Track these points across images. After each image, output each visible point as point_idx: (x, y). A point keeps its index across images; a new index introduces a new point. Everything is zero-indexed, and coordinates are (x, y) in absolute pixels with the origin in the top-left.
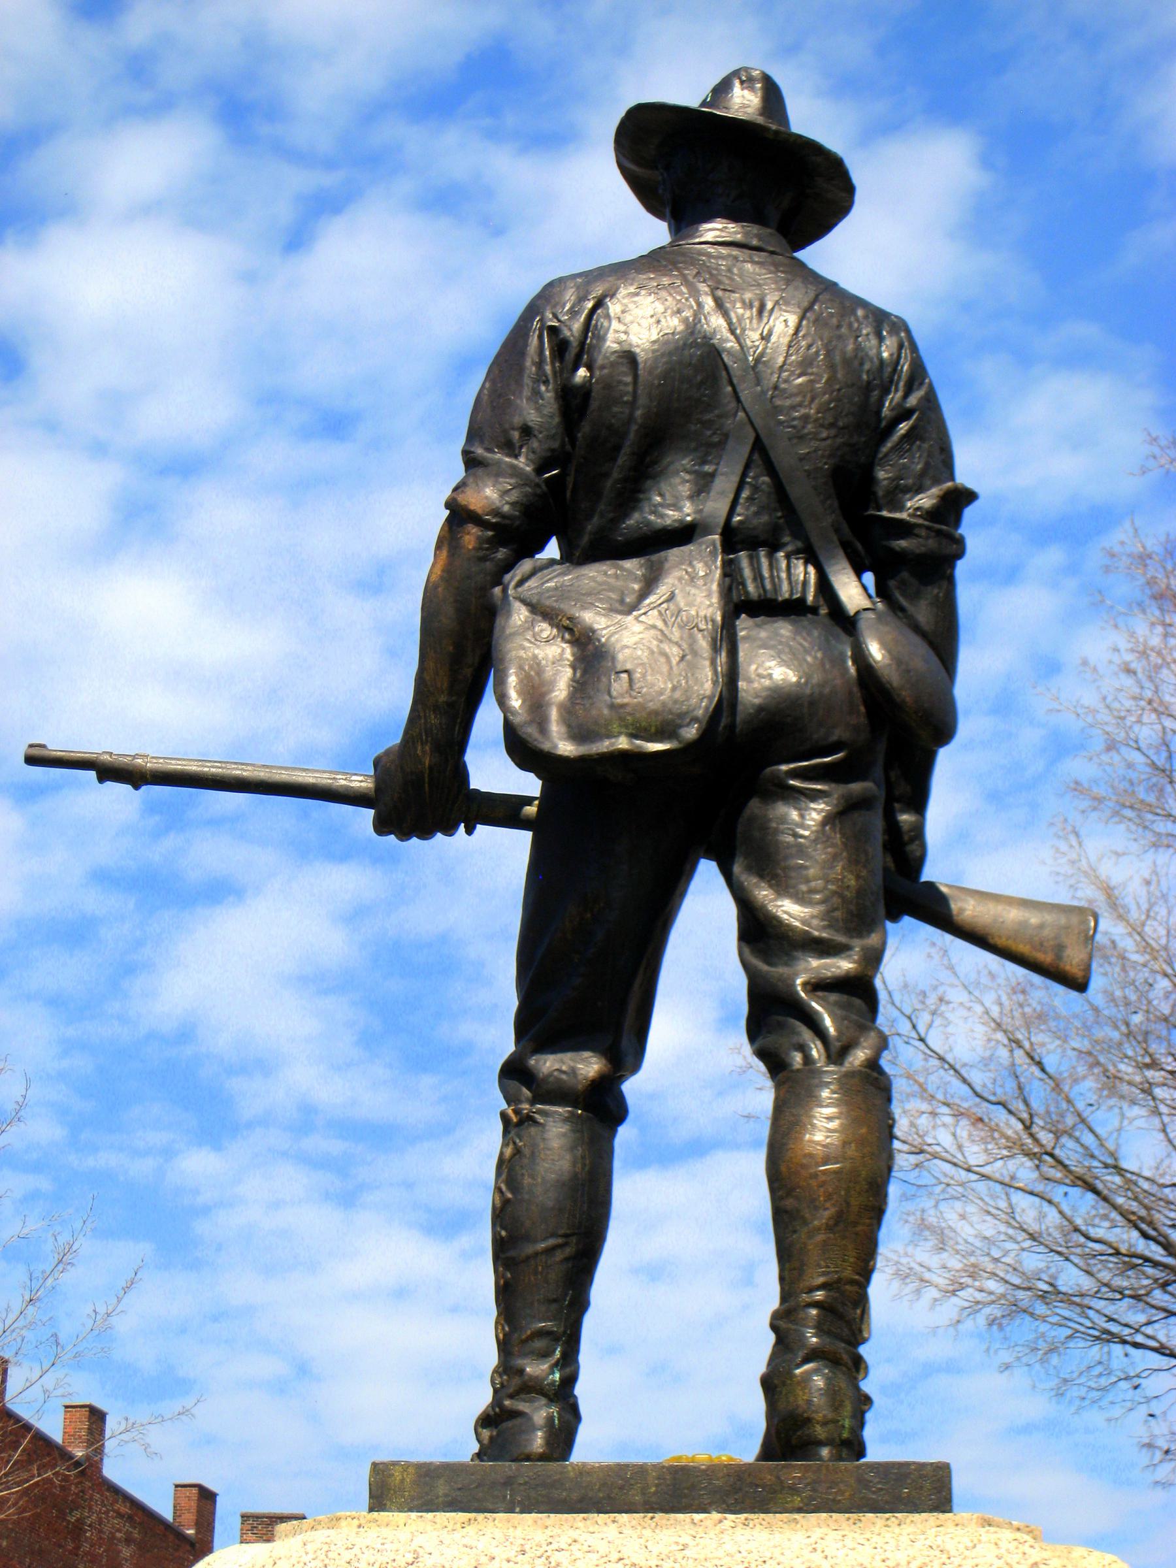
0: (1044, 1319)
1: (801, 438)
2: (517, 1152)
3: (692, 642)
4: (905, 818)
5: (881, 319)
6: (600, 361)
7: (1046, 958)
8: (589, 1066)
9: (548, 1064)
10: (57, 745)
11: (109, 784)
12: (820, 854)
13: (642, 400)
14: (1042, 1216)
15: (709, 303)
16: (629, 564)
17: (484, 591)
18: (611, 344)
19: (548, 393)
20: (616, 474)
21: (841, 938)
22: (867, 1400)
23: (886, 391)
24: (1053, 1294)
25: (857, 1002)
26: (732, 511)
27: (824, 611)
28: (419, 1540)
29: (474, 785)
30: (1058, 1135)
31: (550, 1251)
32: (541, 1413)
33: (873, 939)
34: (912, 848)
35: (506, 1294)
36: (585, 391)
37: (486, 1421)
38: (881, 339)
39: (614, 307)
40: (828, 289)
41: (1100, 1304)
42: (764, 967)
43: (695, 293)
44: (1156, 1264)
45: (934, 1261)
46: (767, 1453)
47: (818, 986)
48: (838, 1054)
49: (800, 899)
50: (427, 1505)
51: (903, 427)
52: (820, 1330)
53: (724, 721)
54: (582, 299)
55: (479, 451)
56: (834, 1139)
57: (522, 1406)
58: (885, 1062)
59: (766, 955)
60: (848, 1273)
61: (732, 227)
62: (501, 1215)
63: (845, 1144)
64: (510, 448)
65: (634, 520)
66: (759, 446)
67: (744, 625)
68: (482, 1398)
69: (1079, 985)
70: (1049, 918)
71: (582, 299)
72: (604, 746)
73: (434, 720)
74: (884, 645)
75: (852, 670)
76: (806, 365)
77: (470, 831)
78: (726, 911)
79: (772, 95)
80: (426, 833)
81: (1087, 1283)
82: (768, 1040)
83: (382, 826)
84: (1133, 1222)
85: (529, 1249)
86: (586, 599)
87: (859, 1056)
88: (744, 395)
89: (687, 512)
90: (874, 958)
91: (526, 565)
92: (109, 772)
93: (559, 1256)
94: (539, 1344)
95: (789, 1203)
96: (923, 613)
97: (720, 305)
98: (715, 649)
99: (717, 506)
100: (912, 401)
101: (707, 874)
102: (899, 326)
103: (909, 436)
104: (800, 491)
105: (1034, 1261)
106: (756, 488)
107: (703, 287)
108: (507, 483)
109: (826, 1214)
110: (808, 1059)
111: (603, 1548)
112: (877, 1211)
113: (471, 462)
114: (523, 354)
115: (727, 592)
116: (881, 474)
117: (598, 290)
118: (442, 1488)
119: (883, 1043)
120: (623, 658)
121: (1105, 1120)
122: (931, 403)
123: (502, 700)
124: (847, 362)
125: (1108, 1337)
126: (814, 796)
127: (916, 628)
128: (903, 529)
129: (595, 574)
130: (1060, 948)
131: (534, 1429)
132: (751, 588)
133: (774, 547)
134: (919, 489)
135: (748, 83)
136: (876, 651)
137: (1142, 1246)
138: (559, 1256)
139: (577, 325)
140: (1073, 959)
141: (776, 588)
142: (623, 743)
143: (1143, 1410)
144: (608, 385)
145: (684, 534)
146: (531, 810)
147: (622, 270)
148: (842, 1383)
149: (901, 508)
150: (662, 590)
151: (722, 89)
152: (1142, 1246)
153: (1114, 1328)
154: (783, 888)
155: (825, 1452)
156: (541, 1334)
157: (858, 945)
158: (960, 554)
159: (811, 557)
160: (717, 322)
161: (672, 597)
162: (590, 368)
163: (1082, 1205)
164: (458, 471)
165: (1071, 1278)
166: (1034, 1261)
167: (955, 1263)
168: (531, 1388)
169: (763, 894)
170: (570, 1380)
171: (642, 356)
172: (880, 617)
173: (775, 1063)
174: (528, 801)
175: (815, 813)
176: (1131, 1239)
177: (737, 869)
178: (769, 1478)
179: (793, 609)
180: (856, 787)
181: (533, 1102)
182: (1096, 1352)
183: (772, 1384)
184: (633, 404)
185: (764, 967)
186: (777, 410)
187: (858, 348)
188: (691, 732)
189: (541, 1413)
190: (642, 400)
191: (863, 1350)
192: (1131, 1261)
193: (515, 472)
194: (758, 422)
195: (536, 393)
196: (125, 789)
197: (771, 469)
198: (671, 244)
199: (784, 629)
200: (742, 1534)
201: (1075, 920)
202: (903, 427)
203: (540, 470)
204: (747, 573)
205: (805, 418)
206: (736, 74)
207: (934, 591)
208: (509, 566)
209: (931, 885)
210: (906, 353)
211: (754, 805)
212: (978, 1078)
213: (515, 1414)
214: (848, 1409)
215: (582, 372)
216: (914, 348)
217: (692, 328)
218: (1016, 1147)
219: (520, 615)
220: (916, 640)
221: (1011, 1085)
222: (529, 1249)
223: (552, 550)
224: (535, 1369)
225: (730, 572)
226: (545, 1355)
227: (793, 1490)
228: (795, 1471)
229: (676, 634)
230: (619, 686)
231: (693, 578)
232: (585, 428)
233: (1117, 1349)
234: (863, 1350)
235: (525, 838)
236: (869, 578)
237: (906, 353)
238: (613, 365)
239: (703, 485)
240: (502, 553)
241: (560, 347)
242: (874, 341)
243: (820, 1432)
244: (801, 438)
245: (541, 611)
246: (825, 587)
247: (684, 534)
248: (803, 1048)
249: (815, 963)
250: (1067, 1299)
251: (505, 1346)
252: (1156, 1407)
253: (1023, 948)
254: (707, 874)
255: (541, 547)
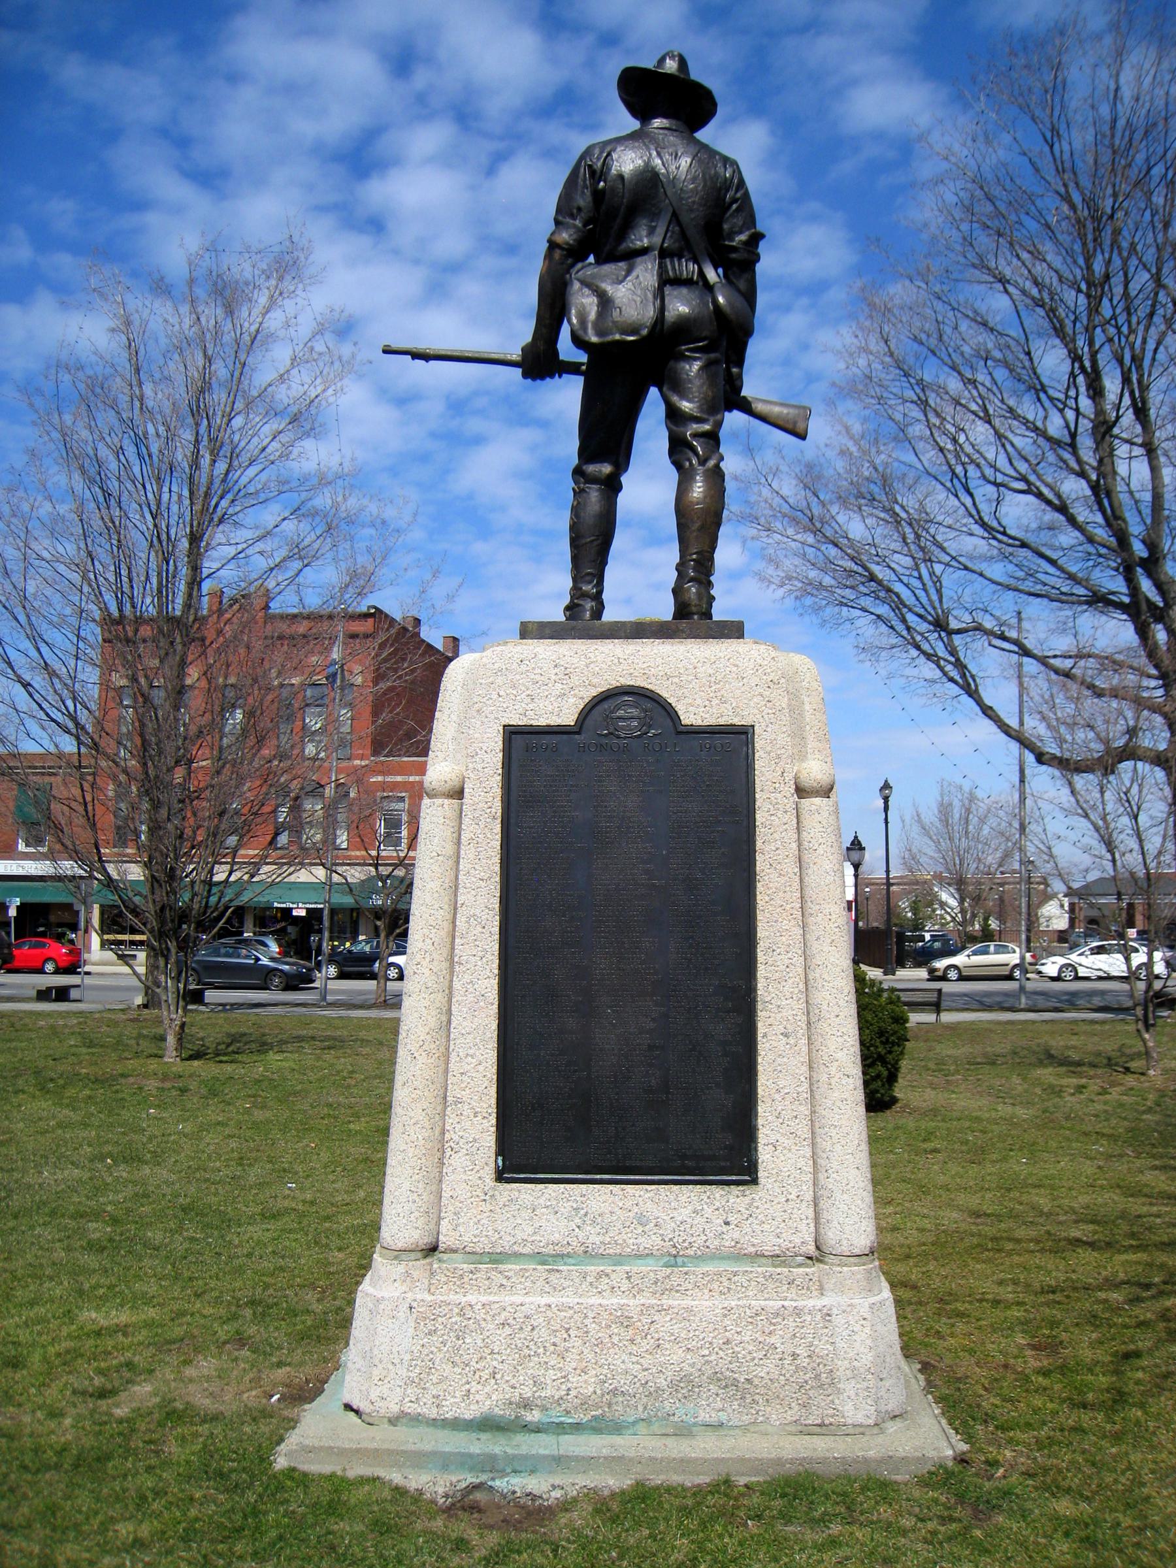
0: (816, 596)
1: (692, 210)
2: (579, 503)
3: (646, 295)
4: (735, 370)
5: (726, 160)
6: (609, 178)
7: (790, 426)
8: (607, 469)
9: (591, 468)
10: (395, 345)
11: (417, 361)
12: (697, 382)
13: (627, 195)
14: (816, 557)
15: (654, 153)
16: (620, 264)
17: (563, 276)
18: (613, 172)
19: (588, 192)
20: (616, 227)
21: (705, 416)
22: (714, 598)
23: (727, 191)
24: (820, 586)
25: (711, 442)
26: (663, 242)
27: (701, 283)
28: (537, 649)
29: (561, 358)
30: (823, 524)
31: (592, 541)
32: (589, 605)
33: (719, 417)
34: (738, 383)
35: (575, 559)
36: (603, 190)
37: (567, 608)
38: (726, 169)
39: (615, 156)
40: (704, 147)
41: (839, 591)
42: (674, 428)
43: (648, 149)
44: (861, 575)
45: (775, 574)
46: (674, 618)
47: (696, 435)
48: (703, 462)
49: (689, 401)
50: (542, 637)
51: (735, 206)
52: (695, 570)
53: (659, 327)
54: (602, 152)
55: (560, 218)
56: (701, 495)
57: (581, 602)
58: (722, 465)
59: (676, 424)
60: (706, 548)
61: (665, 121)
62: (573, 528)
63: (705, 497)
64: (573, 217)
65: (623, 246)
66: (675, 215)
67: (668, 290)
68: (567, 601)
69: (802, 437)
70: (792, 411)
71: (602, 152)
72: (610, 338)
73: (544, 331)
74: (724, 297)
75: (711, 307)
76: (694, 180)
77: (560, 376)
78: (661, 409)
79: (683, 63)
80: (542, 378)
81: (833, 582)
82: (675, 457)
83: (525, 375)
84: (852, 559)
85: (583, 541)
86: (603, 278)
87: (711, 463)
88: (669, 193)
89: (646, 242)
90: (719, 424)
91: (579, 265)
92: (416, 355)
93: (595, 543)
94: (588, 578)
95: (683, 521)
96: (742, 285)
97: (659, 154)
98: (655, 298)
99: (657, 240)
100: (739, 195)
101: (654, 392)
102: (734, 164)
103: (738, 210)
104: (692, 233)
105: (813, 574)
106: (673, 232)
107: (652, 147)
108: (572, 231)
109: (697, 525)
110: (691, 464)
111: (607, 651)
112: (718, 524)
113: (557, 223)
114: (577, 177)
115: (660, 275)
116: (726, 226)
117: (608, 149)
118: (547, 631)
119: (722, 459)
120: (618, 302)
121: (841, 518)
122: (746, 195)
123: (569, 321)
124: (711, 178)
125: (842, 604)
126: (695, 359)
127: (739, 291)
128: (734, 249)
129: (608, 268)
130: (795, 423)
131: (586, 611)
132: (671, 273)
133: (680, 258)
134: (741, 232)
135: (672, 58)
136: (721, 300)
137: (855, 568)
138: (595, 543)
139: (599, 164)
140: (800, 427)
141: (681, 273)
142: (617, 337)
143: (854, 633)
144: (613, 189)
145: (644, 251)
146: (584, 368)
147: (619, 140)
148: (703, 590)
149: (732, 240)
150: (634, 274)
151: (662, 61)
152: (855, 568)
153: (845, 601)
154: (683, 396)
155: (696, 617)
156: (589, 574)
157: (712, 420)
158: (758, 260)
159: (696, 261)
160: (658, 161)
161: (638, 277)
162: (605, 182)
163: (833, 552)
164: (552, 226)
165: (828, 581)
166: (813, 574)
167: (783, 575)
168: (585, 595)
169: (675, 399)
170: (600, 592)
171: (626, 176)
172: (723, 285)
173: (678, 465)
174: (583, 364)
175: (696, 366)
176: (850, 565)
177: (665, 389)
178: (674, 627)
179: (688, 282)
180: (713, 356)
181: (585, 483)
182: (837, 609)
183: (676, 591)
184: (623, 197)
185: (674, 428)
186: (681, 199)
187: (716, 173)
188: (645, 332)
189: (589, 605)
190: (627, 195)
191: (712, 578)
192: (850, 573)
193: (575, 226)
194: (674, 204)
195: (583, 192)
196: (423, 362)
197: (679, 224)
198: (641, 129)
199: (684, 291)
200: (661, 647)
201: (802, 411)
202: (735, 206)
203: (585, 225)
204: (669, 267)
205: (694, 202)
206: (667, 54)
207: (747, 276)
208: (573, 265)
209: (744, 398)
210: (736, 175)
211: (672, 363)
212: (791, 501)
213: (578, 605)
214: (705, 599)
215: (602, 184)
216: (740, 173)
217: (647, 164)
218: (806, 529)
219: (577, 285)
220: (737, 294)
221: (805, 503)
222: (583, 541)
223: (591, 259)
224: (586, 588)
225: (662, 267)
226: (590, 582)
227: (683, 631)
228: (684, 624)
229: (639, 292)
230: (616, 313)
231: (646, 270)
232: (604, 207)
233: (845, 609)
234: (712, 578)
235: (582, 378)
236: (720, 271)
237: (736, 175)
238: (614, 181)
239: (651, 231)
240: (570, 261)
241: (593, 173)
242: (723, 169)
243: (694, 609)
244: (692, 210)
245: (585, 283)
246: (702, 274)
247: (644, 251)
248: (690, 461)
249: (695, 426)
250: (825, 589)
251: (575, 580)
252: (859, 631)
253: (780, 423)
254: (654, 392)
255: (587, 258)
